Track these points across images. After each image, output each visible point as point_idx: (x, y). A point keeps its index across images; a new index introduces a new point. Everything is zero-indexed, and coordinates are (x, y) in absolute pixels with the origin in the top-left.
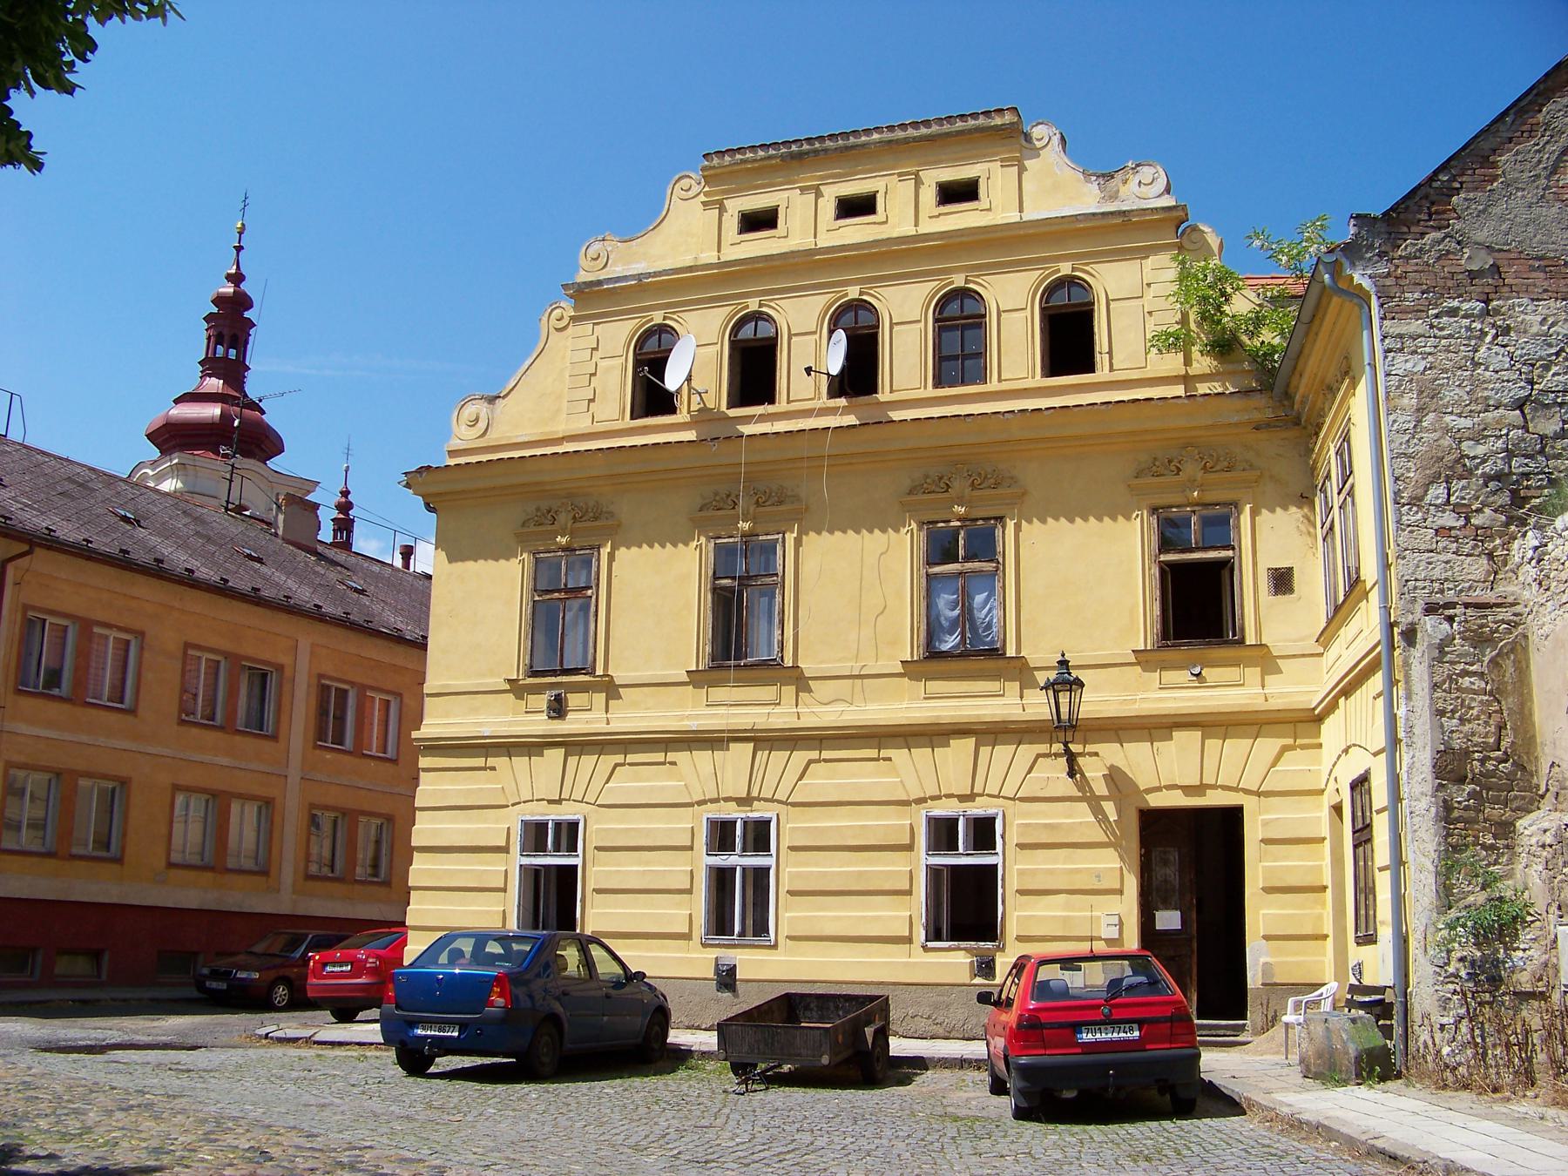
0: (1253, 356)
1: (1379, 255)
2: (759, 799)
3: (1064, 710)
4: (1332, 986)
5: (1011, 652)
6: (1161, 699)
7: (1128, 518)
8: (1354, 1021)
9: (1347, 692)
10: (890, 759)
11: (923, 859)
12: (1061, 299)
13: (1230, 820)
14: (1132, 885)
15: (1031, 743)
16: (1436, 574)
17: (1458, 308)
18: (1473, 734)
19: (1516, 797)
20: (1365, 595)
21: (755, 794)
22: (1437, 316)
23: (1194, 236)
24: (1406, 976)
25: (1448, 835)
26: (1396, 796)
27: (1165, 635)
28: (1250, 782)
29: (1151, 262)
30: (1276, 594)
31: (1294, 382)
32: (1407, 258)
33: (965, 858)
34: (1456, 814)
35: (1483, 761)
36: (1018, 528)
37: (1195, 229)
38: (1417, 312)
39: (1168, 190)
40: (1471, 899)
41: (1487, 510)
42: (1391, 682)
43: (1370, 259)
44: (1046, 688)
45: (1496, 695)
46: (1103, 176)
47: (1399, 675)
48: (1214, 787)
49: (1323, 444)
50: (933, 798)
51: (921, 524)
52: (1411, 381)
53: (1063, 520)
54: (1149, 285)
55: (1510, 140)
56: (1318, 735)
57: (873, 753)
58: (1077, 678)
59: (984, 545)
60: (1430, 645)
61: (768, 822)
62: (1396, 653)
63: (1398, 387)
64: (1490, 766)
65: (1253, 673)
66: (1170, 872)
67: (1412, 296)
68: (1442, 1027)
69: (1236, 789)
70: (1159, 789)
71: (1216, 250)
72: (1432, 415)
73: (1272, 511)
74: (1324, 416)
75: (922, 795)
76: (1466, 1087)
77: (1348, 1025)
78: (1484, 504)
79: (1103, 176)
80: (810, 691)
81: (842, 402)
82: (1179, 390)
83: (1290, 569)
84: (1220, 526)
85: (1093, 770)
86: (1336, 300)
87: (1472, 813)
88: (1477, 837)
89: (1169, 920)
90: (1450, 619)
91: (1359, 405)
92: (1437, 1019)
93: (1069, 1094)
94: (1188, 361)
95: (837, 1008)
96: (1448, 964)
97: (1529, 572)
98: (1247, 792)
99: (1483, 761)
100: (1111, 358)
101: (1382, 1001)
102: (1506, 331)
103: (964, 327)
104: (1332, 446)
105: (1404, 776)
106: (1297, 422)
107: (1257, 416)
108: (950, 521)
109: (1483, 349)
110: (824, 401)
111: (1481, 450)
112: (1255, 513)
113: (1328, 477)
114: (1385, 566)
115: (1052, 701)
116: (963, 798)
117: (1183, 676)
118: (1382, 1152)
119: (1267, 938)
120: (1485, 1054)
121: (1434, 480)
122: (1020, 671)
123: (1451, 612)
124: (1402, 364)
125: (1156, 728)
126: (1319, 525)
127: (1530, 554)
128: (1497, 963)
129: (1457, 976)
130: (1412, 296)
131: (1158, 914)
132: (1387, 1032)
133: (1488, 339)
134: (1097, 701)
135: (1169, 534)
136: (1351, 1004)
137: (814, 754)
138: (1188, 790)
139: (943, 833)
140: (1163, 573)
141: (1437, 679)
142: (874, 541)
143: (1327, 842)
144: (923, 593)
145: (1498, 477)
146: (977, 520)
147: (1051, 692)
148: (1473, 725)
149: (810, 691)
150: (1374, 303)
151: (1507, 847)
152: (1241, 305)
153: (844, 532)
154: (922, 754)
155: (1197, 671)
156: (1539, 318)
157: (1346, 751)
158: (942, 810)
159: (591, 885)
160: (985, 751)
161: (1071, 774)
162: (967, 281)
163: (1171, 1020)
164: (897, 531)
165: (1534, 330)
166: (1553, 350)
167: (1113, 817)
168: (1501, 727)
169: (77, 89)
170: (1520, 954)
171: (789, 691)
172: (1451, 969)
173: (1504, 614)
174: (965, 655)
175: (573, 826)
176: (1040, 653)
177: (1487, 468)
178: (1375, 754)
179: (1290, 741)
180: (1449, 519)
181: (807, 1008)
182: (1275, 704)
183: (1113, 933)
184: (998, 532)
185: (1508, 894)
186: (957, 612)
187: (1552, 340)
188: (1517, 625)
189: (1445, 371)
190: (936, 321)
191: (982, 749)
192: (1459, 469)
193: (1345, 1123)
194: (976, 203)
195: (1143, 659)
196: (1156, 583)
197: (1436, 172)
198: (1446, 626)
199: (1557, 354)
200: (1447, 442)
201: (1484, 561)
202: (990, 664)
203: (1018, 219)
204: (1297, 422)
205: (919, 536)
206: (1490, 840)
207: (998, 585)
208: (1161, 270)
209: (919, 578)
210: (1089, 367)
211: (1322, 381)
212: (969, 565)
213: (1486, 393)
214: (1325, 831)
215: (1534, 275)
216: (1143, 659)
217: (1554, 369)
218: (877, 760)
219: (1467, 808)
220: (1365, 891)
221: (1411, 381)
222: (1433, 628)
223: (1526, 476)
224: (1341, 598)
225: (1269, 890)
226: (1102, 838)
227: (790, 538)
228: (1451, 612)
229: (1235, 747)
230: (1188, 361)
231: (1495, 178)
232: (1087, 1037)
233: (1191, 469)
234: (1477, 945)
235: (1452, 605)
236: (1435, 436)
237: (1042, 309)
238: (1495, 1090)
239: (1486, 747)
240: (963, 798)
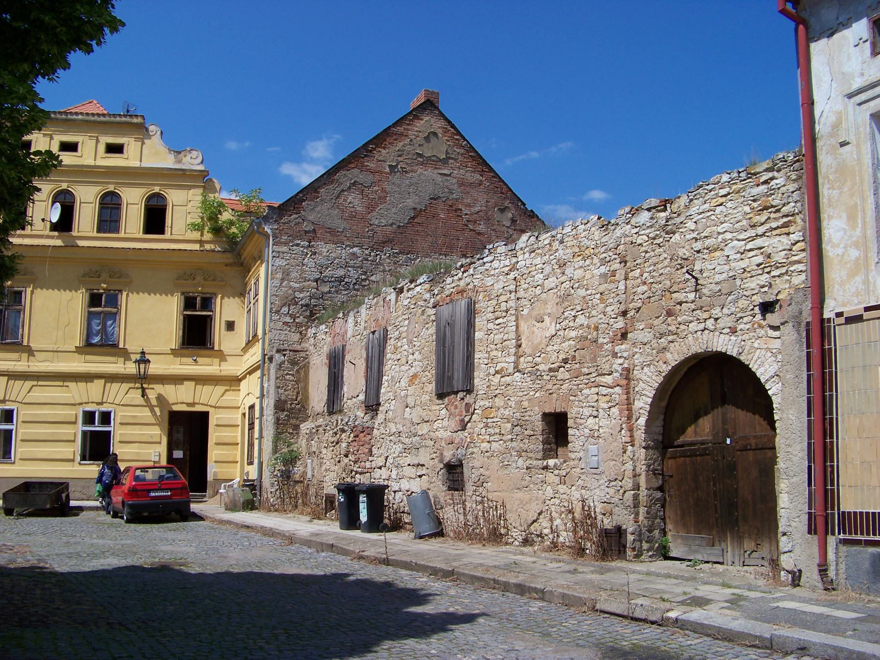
0: (228, 236)
1: (275, 221)
2: (9, 401)
3: (142, 371)
4: (238, 479)
5: (121, 346)
6: (180, 369)
7: (172, 295)
8: (243, 490)
9: (250, 373)
10: (68, 386)
11: (80, 427)
12: (154, 202)
13: (203, 417)
14: (165, 440)
15: (127, 383)
16: (282, 338)
17: (300, 244)
18: (288, 395)
19: (301, 417)
20: (258, 341)
21: (7, 398)
22: (292, 246)
23: (210, 183)
24: (262, 476)
25: (277, 429)
26: (262, 415)
27: (183, 343)
28: (212, 402)
29: (192, 191)
30: (228, 331)
31: (242, 251)
32: (284, 223)
33: (98, 428)
34: (280, 422)
35: (291, 404)
36: (127, 295)
37: (211, 180)
38: (286, 244)
39: (202, 162)
40: (283, 450)
41: (301, 317)
42: (263, 375)
43: (271, 222)
44: (135, 362)
45: (297, 382)
46: (177, 152)
47: (266, 373)
48: (199, 404)
49: (250, 277)
50: (86, 403)
51: (87, 290)
52: (280, 269)
53: (146, 293)
54: (190, 201)
55: (325, 184)
56: (239, 386)
57: (61, 383)
58: (148, 359)
59: (113, 301)
60: (277, 364)
61: (12, 411)
62: (266, 365)
63: (276, 270)
64: (293, 406)
65: (216, 361)
66: (179, 436)
67: (285, 238)
68: (271, 492)
69: (207, 405)
70: (177, 404)
71: (218, 190)
72: (286, 282)
73: (229, 298)
74: (252, 268)
75: (81, 402)
76: (276, 511)
77: (241, 492)
78: (300, 315)
79: (177, 152)
80: (34, 356)
81: (56, 233)
82: (197, 247)
83: (234, 321)
84: (207, 303)
85: (152, 395)
86: (257, 236)
87: (286, 422)
88: (287, 430)
89: (178, 454)
90: (284, 355)
91: (262, 270)
92: (270, 490)
93: (146, 514)
94: (202, 235)
95: (47, 487)
96: (274, 472)
97: (312, 341)
98: (211, 406)
99: (291, 404)
100: (171, 230)
101: (253, 484)
102: (315, 253)
103: (112, 208)
104: (253, 280)
105: (265, 408)
106: (242, 264)
107: (227, 261)
108: (99, 290)
109: (306, 259)
110: (47, 232)
111: (301, 295)
112: (222, 298)
113: (251, 290)
114: (265, 334)
115: (137, 367)
116: (98, 404)
117: (189, 360)
118: (245, 526)
119: (215, 462)
120: (284, 501)
121: (284, 305)
122: (125, 354)
123: (285, 353)
124: (279, 262)
125: (177, 380)
126: (246, 307)
127: (312, 335)
128: (290, 472)
129: (277, 475)
130: (285, 238)
131: (174, 452)
132: (255, 495)
133: (309, 256)
134: (156, 367)
135: (189, 303)
136: (244, 486)
137: (35, 383)
138: (188, 404)
139: (89, 418)
140: (184, 318)
141: (278, 376)
142: (66, 295)
143: (240, 427)
144: (86, 319)
145: (307, 305)
146: (111, 290)
147: (137, 364)
148: (289, 392)
149: (34, 356)
150: (271, 237)
151: (297, 433)
152: (226, 216)
153: (53, 290)
154: (82, 385)
155: (195, 358)
156: (326, 250)
157: (248, 394)
158: (89, 408)
159: (20, 437)
160: (108, 385)
161: (143, 396)
162: (115, 189)
163: (181, 489)
164: (76, 291)
165: (324, 254)
166: (330, 262)
167: (158, 414)
168: (298, 393)
170: (296, 468)
171: (25, 356)
172: (275, 473)
173: (303, 354)
174: (102, 346)
175: (109, 413)
176: (133, 346)
177: (303, 302)
178: (257, 398)
179: (228, 388)
180: (288, 319)
181: (34, 487)
182: (224, 373)
183: (157, 459)
184: (119, 296)
185: (295, 449)
186: (99, 327)
187: (330, 258)
188: (306, 358)
189: (292, 266)
190: (100, 204)
191: (107, 384)
192: (294, 302)
193: (236, 520)
194: (122, 155)
195: (174, 352)
196: (182, 322)
197: (298, 193)
198: (283, 357)
199: (331, 264)
200: (290, 292)
201: (298, 334)
202: (112, 350)
203: (139, 166)
204: (242, 264)
205: (86, 295)
206: (291, 431)
207: (118, 318)
208: (195, 196)
209: (85, 312)
210: (162, 232)
211: (252, 255)
212: (106, 309)
213: (305, 276)
214: (239, 423)
215: (327, 234)
216: (174, 352)
217: (329, 269)
218: (63, 386)
219: (284, 420)
220: (251, 445)
221: (280, 269)
222: (278, 358)
223: (316, 306)
224: (251, 339)
225: (217, 444)
226: (153, 421)
227: (29, 290)
228: (285, 353)
229: (207, 389)
230: (202, 235)
231: (318, 197)
232: (152, 494)
233: (199, 278)
234: (284, 465)
235: (286, 350)
236: (286, 289)
237: (146, 205)
238: (285, 511)
239: (292, 400)
240: (98, 404)
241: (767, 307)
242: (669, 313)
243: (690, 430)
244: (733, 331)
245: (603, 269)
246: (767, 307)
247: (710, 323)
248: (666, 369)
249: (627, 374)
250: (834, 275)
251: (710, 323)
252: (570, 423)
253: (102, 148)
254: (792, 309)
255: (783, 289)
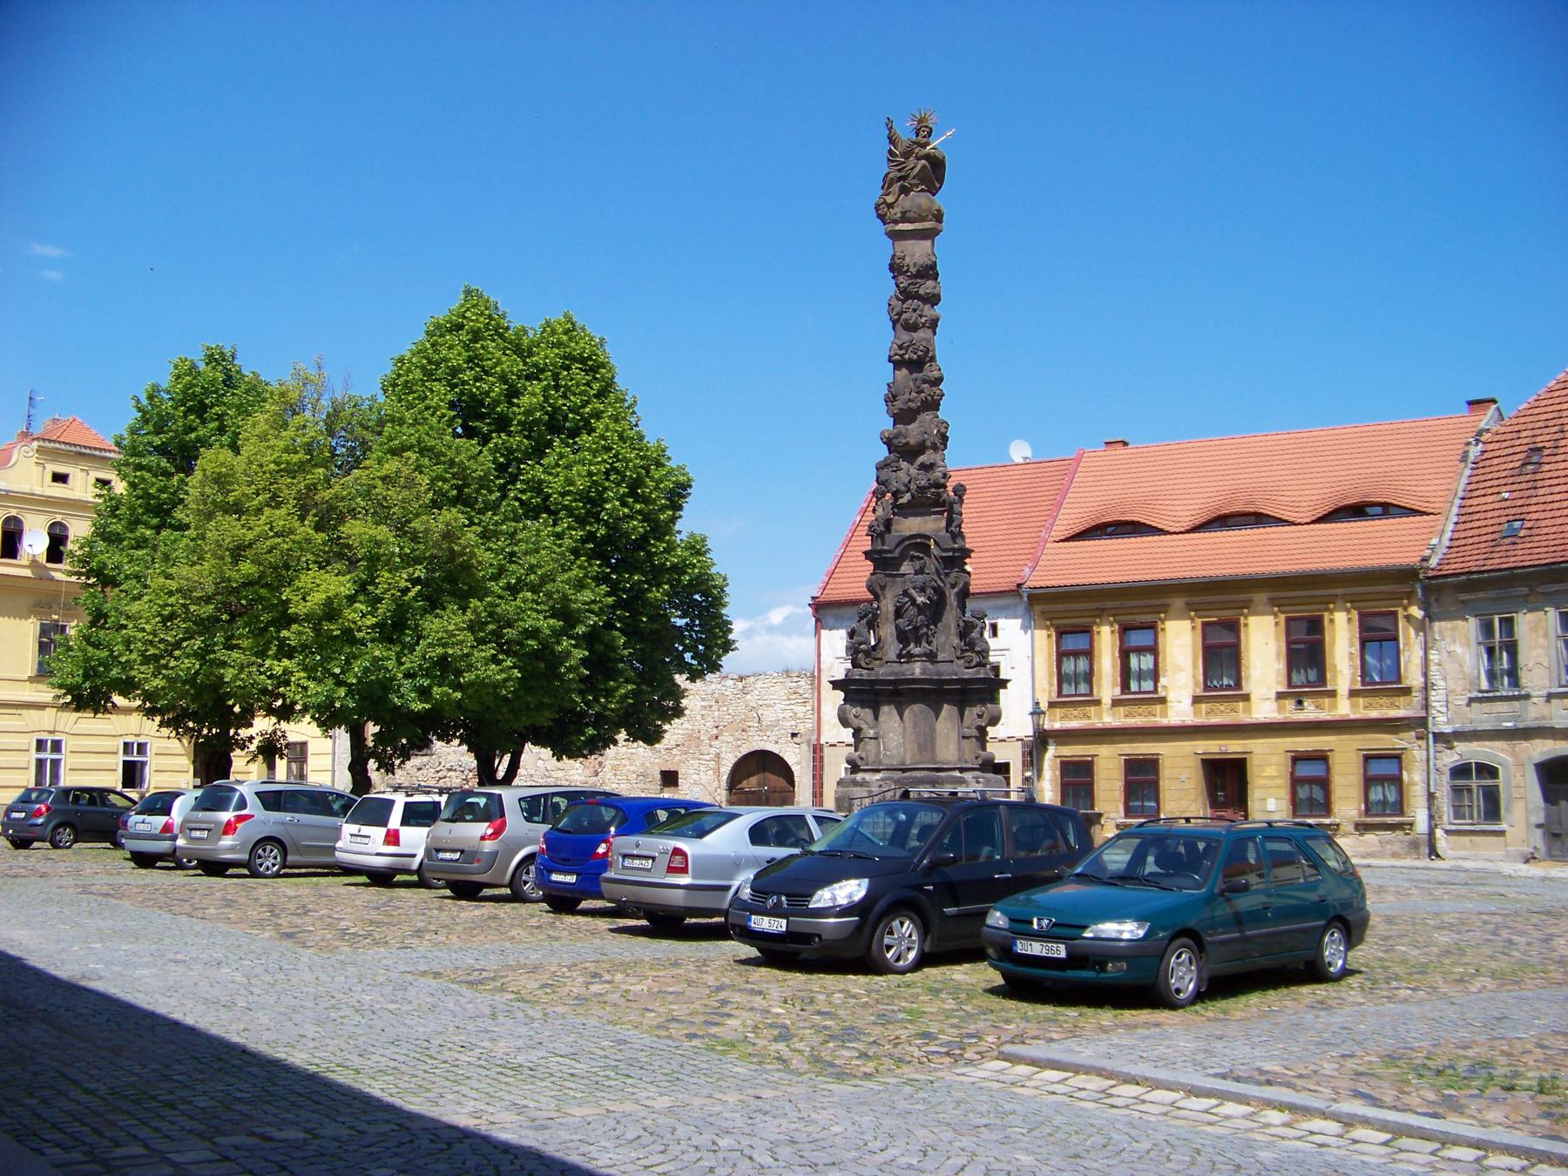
61: (146, 744)
116: (136, 735)
139: (127, 747)
158: (129, 739)
169: (1425, 741)
175: (145, 744)
240: (136, 735)
241: (794, 735)
242: (743, 730)
243: (745, 782)
244: (777, 742)
245: (704, 703)
246: (794, 735)
247: (765, 738)
248: (740, 755)
249: (718, 755)
250: (824, 727)
251: (765, 738)
252: (680, 776)
253: (49, 477)
254: (806, 738)
255: (801, 729)
